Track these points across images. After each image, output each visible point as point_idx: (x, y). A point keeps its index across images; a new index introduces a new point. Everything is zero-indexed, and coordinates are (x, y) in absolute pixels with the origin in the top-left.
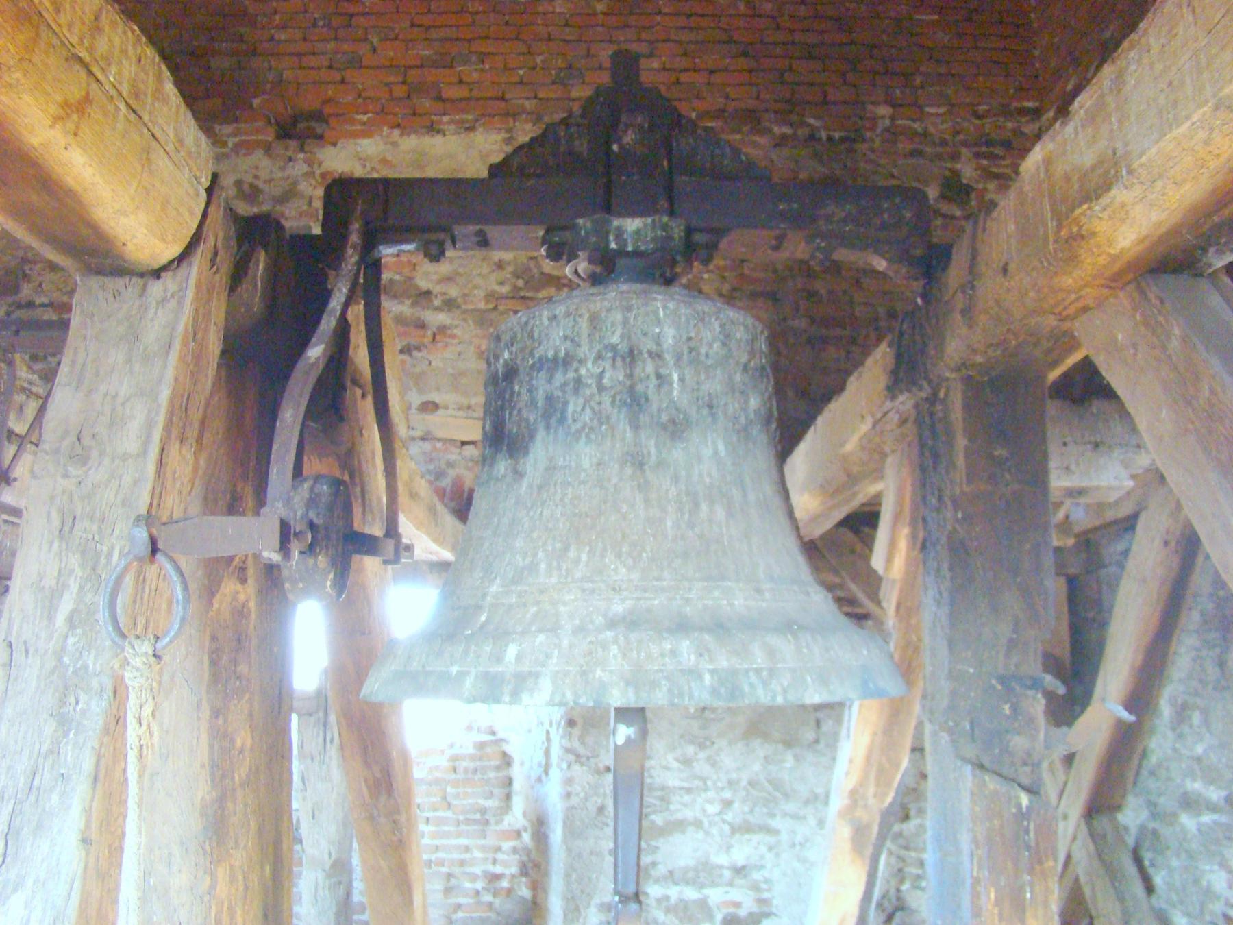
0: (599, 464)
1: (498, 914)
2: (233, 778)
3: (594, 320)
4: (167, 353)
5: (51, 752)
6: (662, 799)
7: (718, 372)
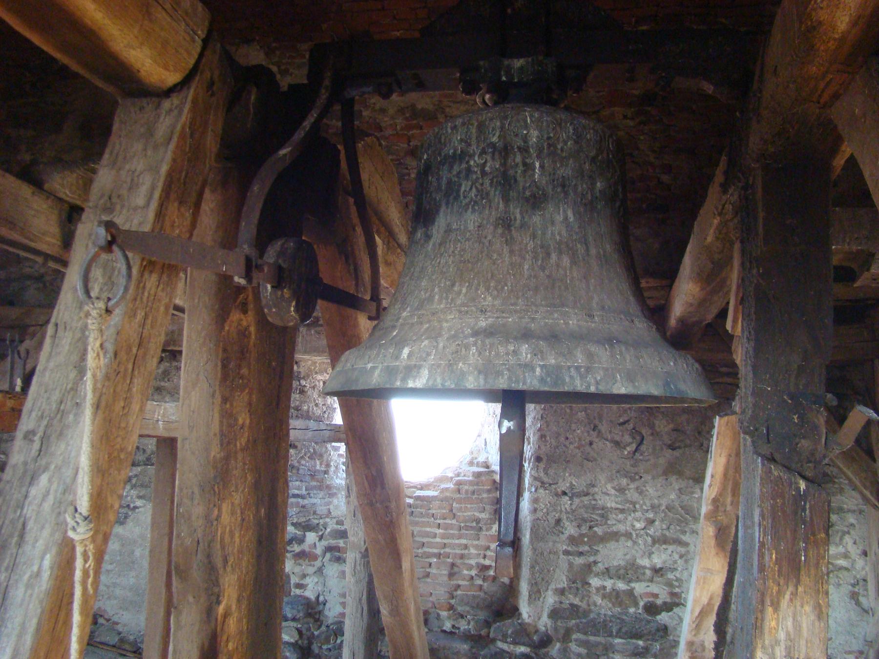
0: (479, 227)
1: (485, 593)
2: (235, 445)
3: (481, 127)
4: (168, 143)
5: (72, 389)
6: (602, 516)
7: (571, 161)
